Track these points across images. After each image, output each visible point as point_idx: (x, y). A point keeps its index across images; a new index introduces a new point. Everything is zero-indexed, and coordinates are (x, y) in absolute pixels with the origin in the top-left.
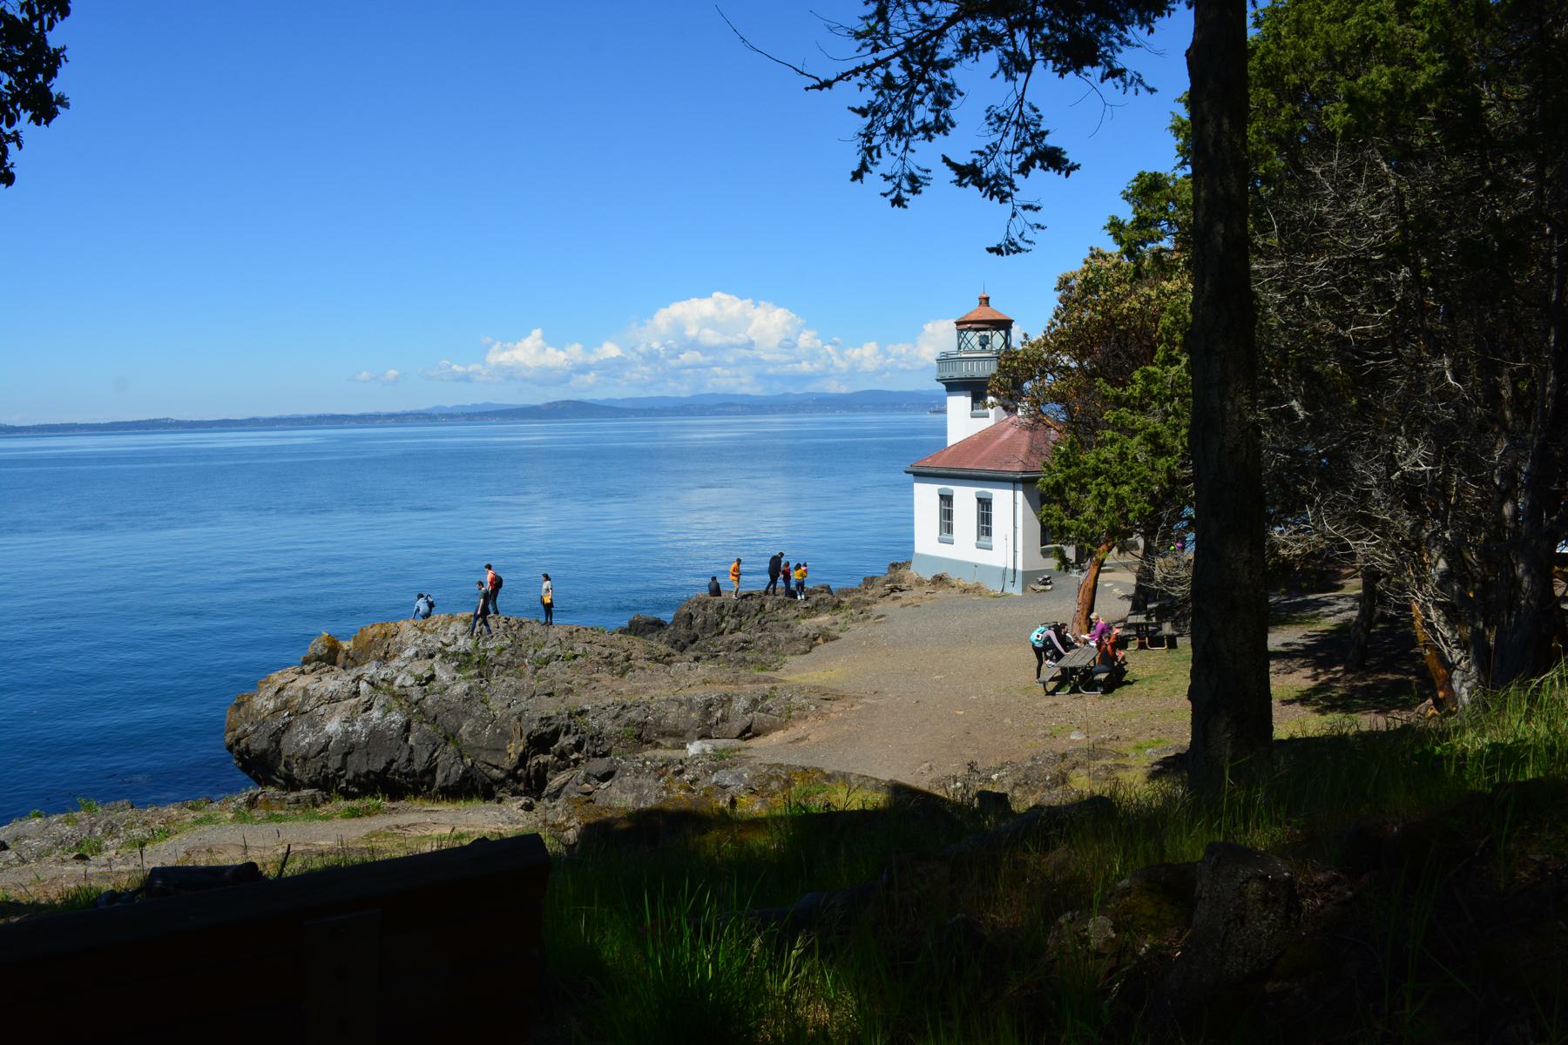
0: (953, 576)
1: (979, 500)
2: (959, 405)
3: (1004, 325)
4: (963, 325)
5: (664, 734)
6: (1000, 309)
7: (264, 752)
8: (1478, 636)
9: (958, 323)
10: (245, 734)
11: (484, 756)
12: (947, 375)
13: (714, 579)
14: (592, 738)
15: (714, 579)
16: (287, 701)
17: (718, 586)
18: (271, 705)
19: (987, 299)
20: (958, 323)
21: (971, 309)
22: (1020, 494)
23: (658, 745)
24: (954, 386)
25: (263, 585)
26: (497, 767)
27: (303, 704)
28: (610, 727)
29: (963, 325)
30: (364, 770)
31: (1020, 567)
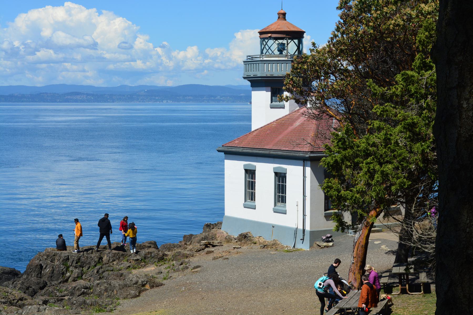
0: (255, 234)
1: (276, 174)
3: (298, 35)
6: (294, 22)
12: (252, 74)
19: (284, 14)
21: (271, 21)
22: (308, 169)
24: (257, 83)
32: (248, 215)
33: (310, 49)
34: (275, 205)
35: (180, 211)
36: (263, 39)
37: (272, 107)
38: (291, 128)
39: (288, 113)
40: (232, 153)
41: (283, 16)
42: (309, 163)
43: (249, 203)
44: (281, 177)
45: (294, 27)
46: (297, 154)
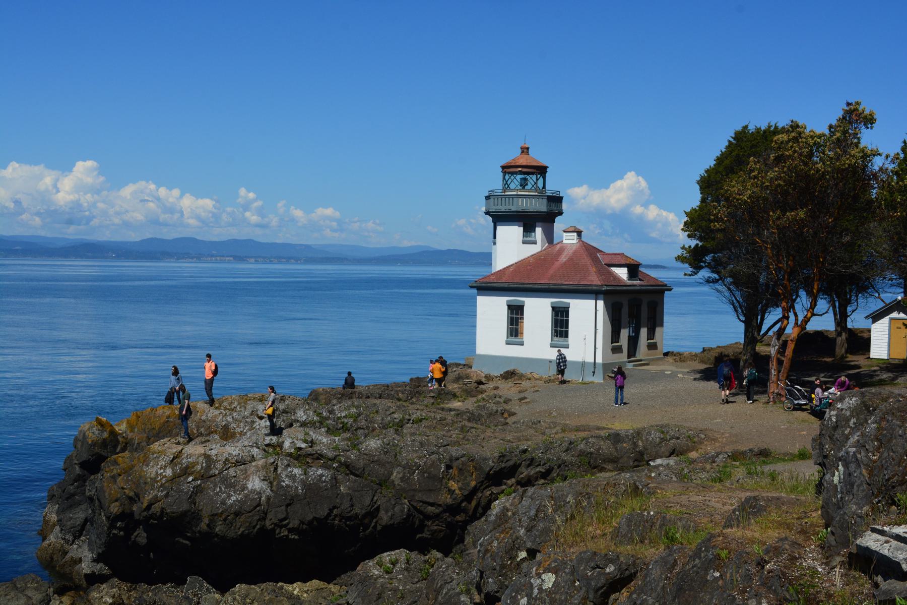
0: (521, 370)
1: (554, 308)
2: (511, 233)
3: (542, 170)
4: (507, 169)
5: (604, 461)
6: (538, 157)
7: (184, 514)
8: (539, 448)
9: (503, 167)
10: (156, 500)
11: (419, 496)
12: (493, 209)
13: (349, 374)
14: (559, 466)
15: (349, 374)
16: (187, 467)
17: (353, 379)
18: (169, 472)
19: (528, 149)
20: (503, 167)
21: (512, 155)
22: (601, 303)
23: (602, 470)
24: (500, 218)
25: (159, 350)
26: (432, 505)
27: (208, 467)
28: (566, 457)
29: (507, 169)
30: (310, 517)
31: (599, 360)
32: (514, 351)
33: (869, 121)
34: (552, 340)
35: (251, 343)
36: (505, 173)
37: (524, 243)
38: (557, 264)
39: (539, 250)
40: (488, 288)
41: (525, 150)
42: (602, 296)
43: (559, 341)
44: (516, 313)
45: (537, 161)
46: (590, 288)
